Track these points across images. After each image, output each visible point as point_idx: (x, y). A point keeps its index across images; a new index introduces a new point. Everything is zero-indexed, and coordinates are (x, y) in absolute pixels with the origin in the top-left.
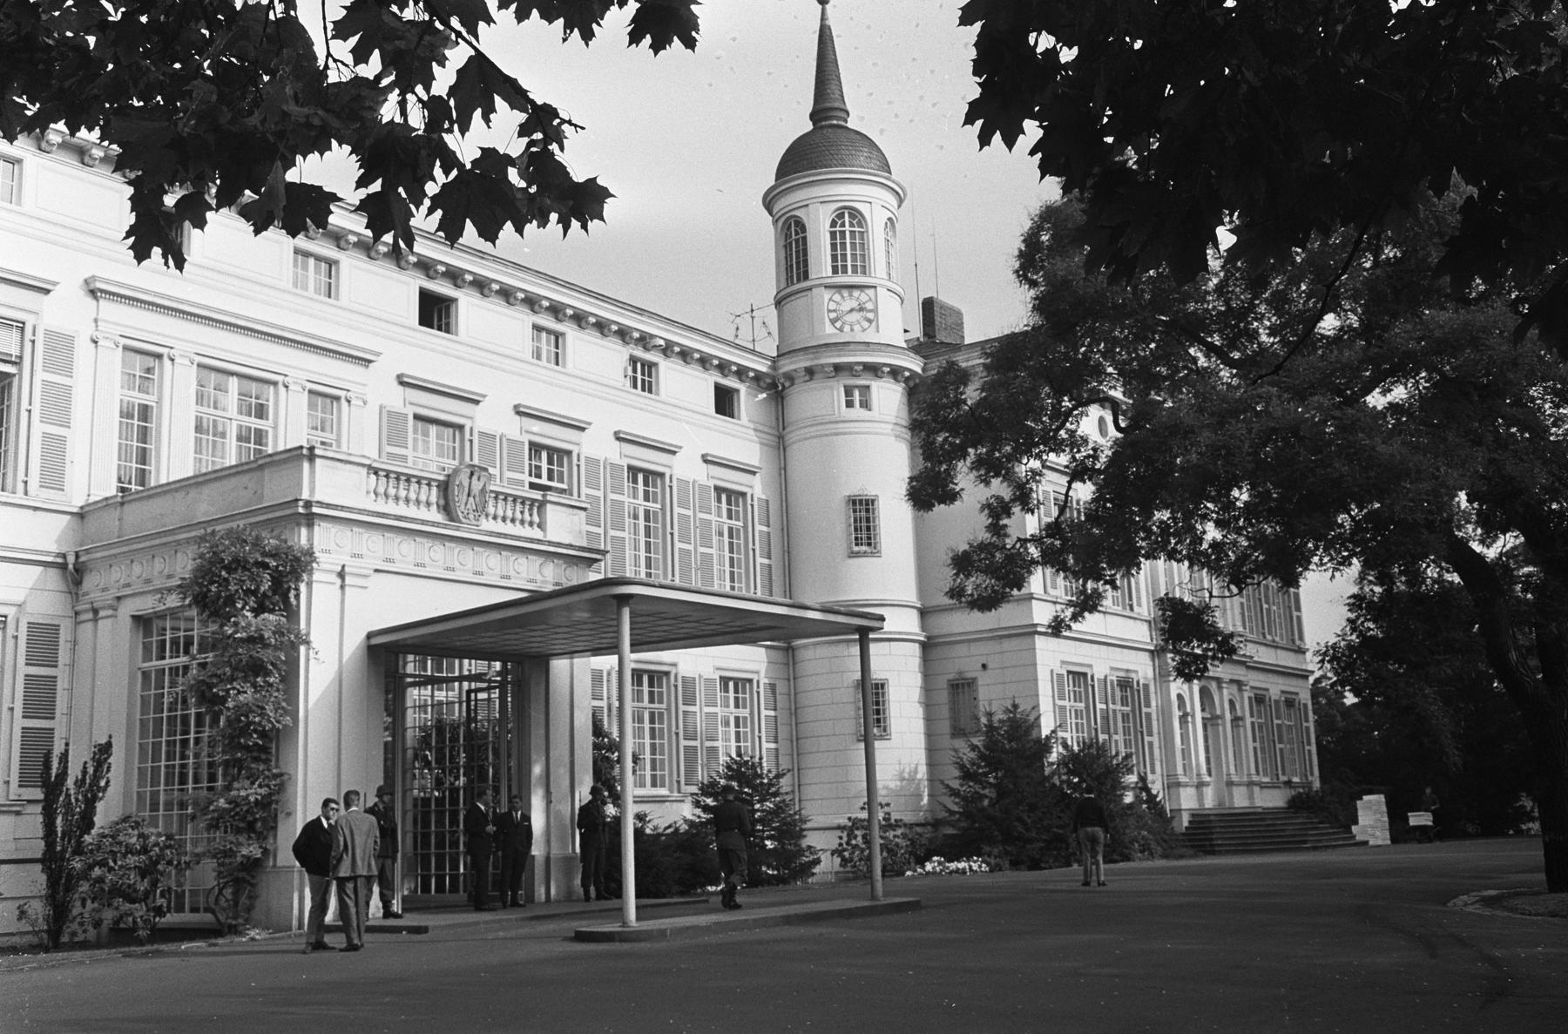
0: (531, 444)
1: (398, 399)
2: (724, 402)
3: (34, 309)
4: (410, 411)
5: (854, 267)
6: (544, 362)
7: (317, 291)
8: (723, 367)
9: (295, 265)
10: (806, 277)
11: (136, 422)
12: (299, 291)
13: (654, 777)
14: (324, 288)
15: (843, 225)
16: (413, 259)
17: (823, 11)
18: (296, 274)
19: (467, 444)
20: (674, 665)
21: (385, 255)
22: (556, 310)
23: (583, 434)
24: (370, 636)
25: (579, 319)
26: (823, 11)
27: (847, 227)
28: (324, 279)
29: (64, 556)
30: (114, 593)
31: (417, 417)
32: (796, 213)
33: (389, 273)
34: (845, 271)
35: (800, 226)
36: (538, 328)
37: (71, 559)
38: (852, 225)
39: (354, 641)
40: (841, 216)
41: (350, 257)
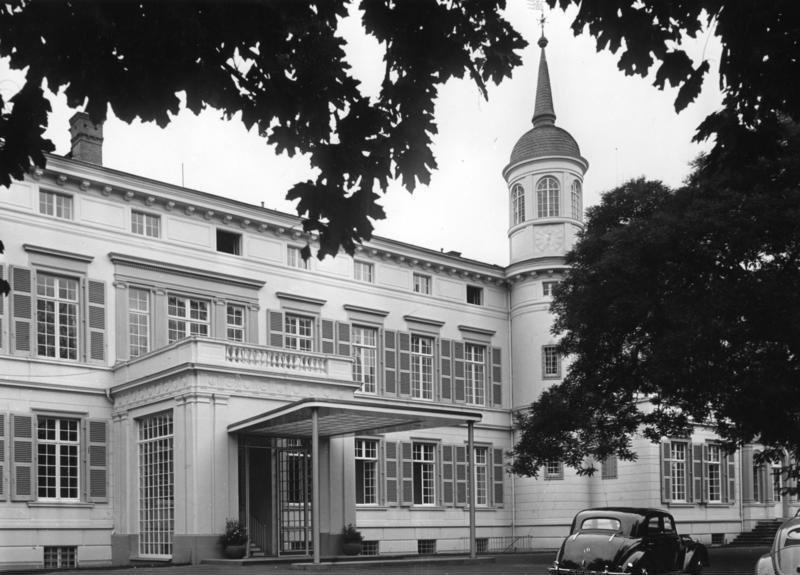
0: (466, 344)
1: (277, 306)
2: (474, 296)
3: (83, 270)
4: (350, 323)
5: (551, 212)
6: (420, 293)
7: (365, 279)
8: (471, 275)
9: (289, 254)
10: (524, 220)
11: (46, 312)
12: (152, 238)
13: (679, 495)
14: (368, 278)
15: (546, 187)
16: (360, 248)
17: (543, 56)
18: (289, 258)
19: (82, 289)
20: (439, 440)
21: (316, 241)
22: (421, 264)
23: (89, 266)
24: (229, 427)
25: (434, 267)
26: (543, 56)
27: (548, 189)
28: (367, 272)
29: (105, 390)
30: (126, 408)
31: (354, 325)
32: (519, 182)
33: (199, 223)
34: (546, 215)
35: (521, 189)
36: (415, 275)
37: (108, 392)
38: (550, 186)
39: (221, 430)
40: (545, 182)
41: (249, 232)
